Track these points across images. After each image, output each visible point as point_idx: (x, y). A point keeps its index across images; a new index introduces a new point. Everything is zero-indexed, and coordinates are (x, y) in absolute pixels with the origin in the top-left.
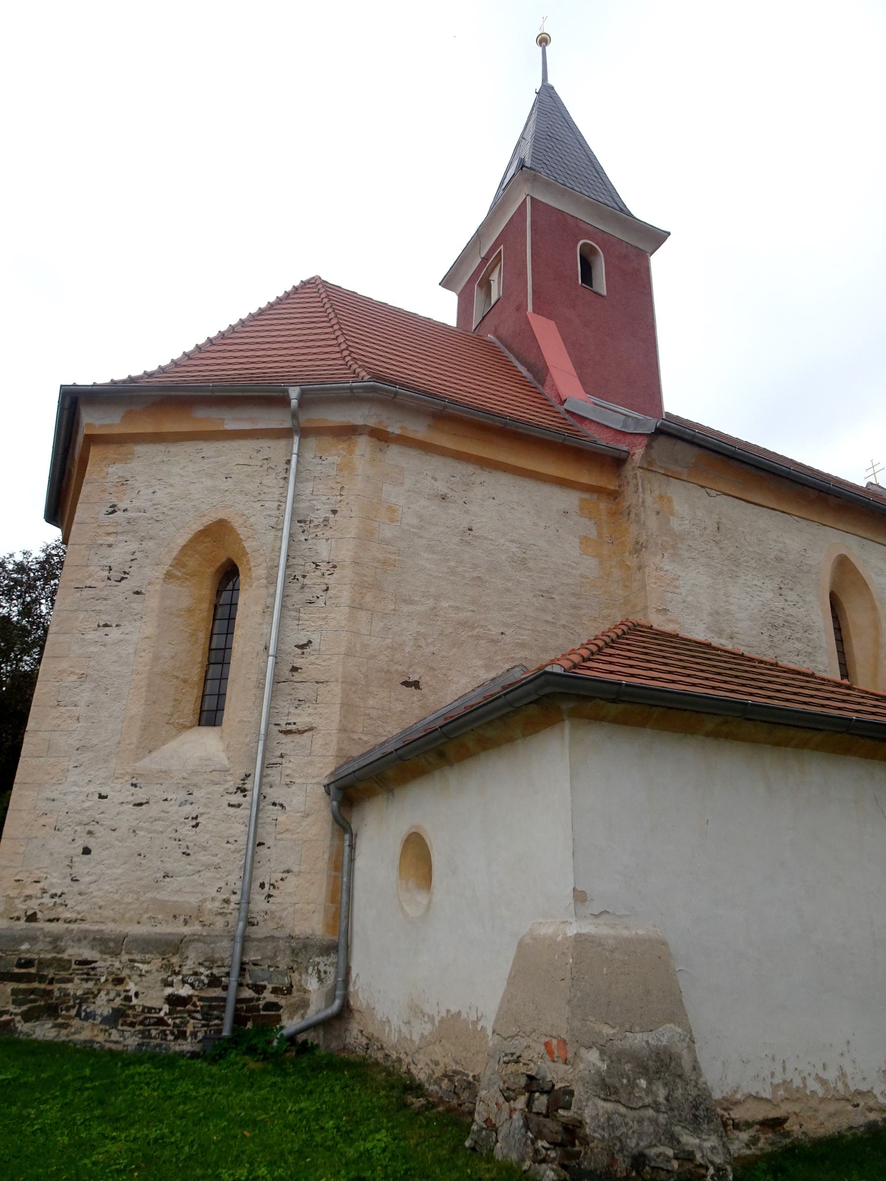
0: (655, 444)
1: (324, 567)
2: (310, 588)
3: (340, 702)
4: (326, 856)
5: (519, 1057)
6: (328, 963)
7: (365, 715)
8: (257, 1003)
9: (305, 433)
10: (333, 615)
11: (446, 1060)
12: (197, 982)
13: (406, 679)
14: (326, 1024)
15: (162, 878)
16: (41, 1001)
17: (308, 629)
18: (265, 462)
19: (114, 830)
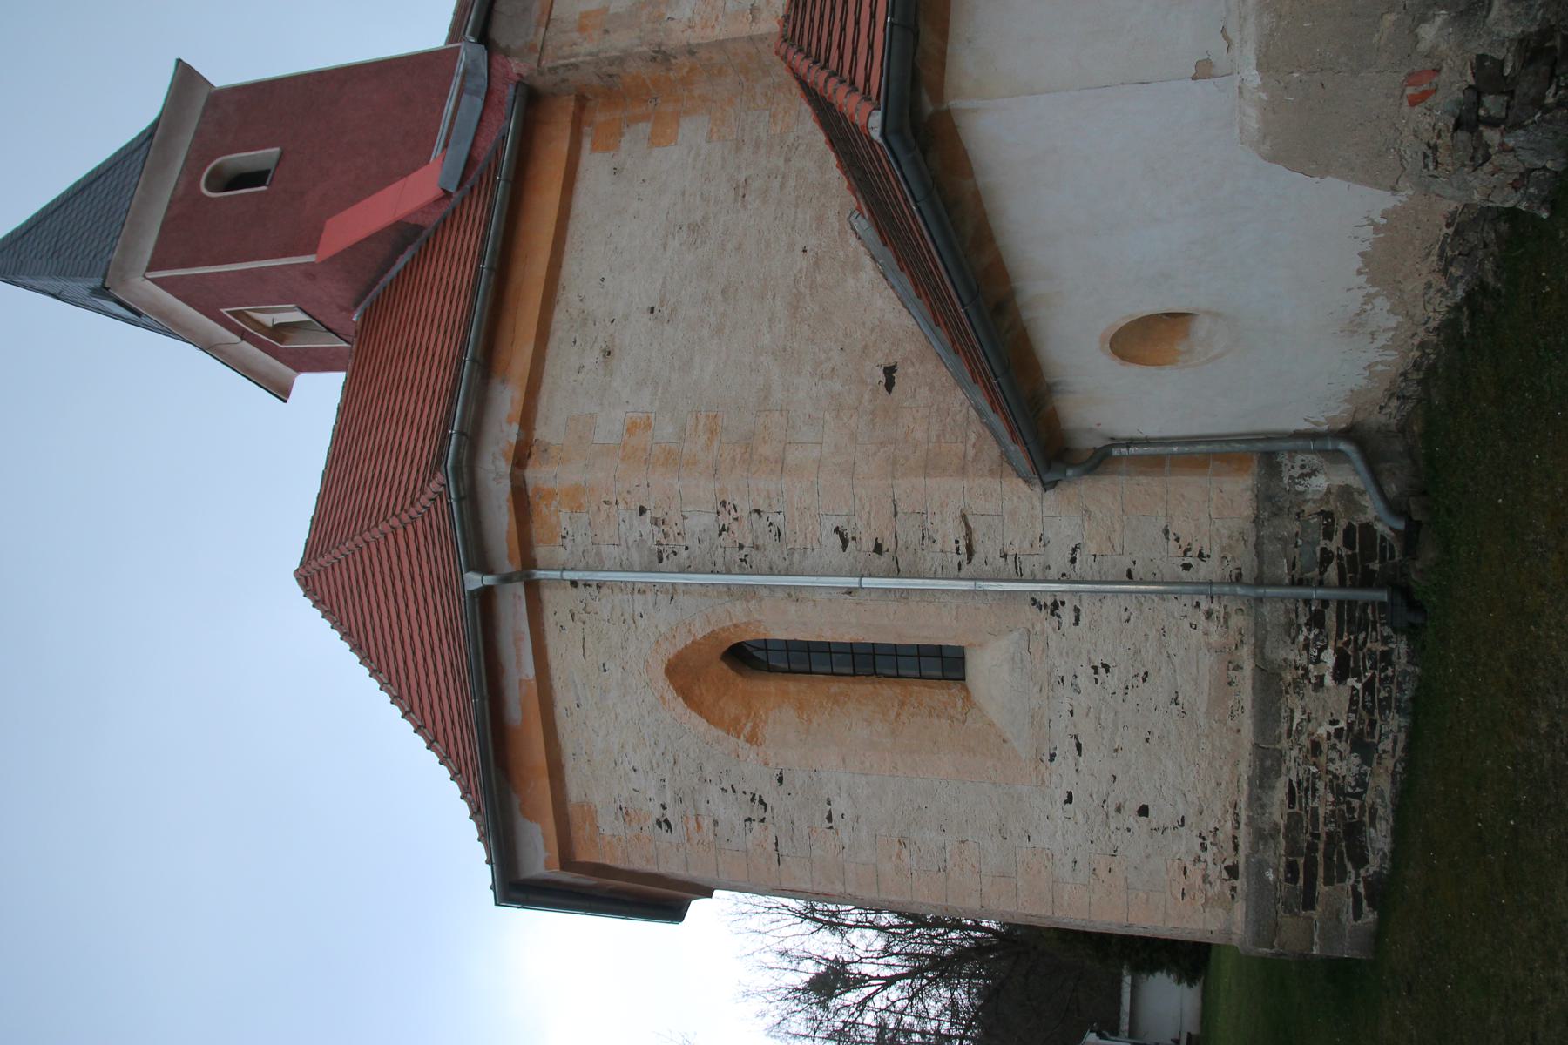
0: (502, 44)
1: (725, 519)
2: (757, 537)
3: (922, 479)
4: (1143, 479)
5: (1428, 144)
6: (1290, 464)
7: (938, 441)
8: (1345, 559)
9: (528, 562)
10: (796, 499)
11: (1424, 271)
12: (1318, 643)
13: (882, 387)
14: (1373, 461)
15: (1179, 707)
16: (1341, 846)
17: (818, 534)
18: (576, 618)
19: (1115, 777)
